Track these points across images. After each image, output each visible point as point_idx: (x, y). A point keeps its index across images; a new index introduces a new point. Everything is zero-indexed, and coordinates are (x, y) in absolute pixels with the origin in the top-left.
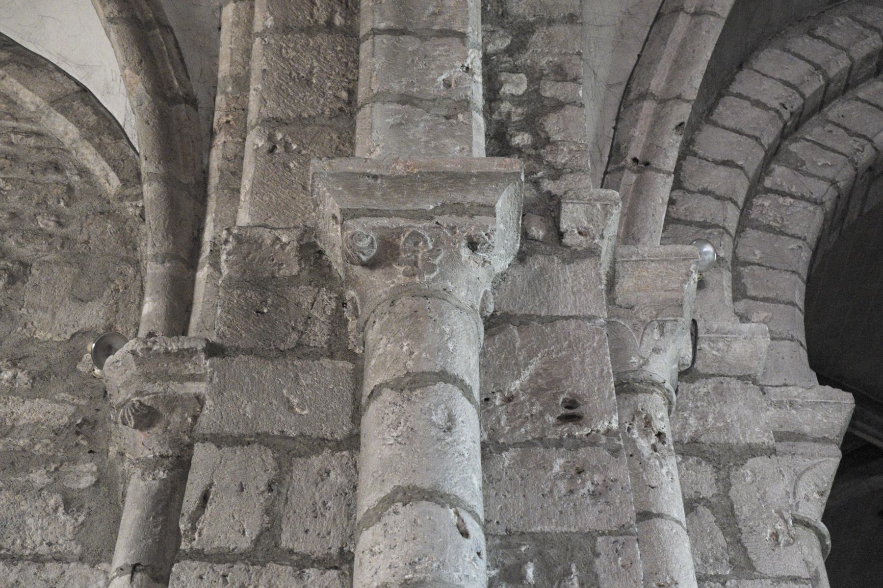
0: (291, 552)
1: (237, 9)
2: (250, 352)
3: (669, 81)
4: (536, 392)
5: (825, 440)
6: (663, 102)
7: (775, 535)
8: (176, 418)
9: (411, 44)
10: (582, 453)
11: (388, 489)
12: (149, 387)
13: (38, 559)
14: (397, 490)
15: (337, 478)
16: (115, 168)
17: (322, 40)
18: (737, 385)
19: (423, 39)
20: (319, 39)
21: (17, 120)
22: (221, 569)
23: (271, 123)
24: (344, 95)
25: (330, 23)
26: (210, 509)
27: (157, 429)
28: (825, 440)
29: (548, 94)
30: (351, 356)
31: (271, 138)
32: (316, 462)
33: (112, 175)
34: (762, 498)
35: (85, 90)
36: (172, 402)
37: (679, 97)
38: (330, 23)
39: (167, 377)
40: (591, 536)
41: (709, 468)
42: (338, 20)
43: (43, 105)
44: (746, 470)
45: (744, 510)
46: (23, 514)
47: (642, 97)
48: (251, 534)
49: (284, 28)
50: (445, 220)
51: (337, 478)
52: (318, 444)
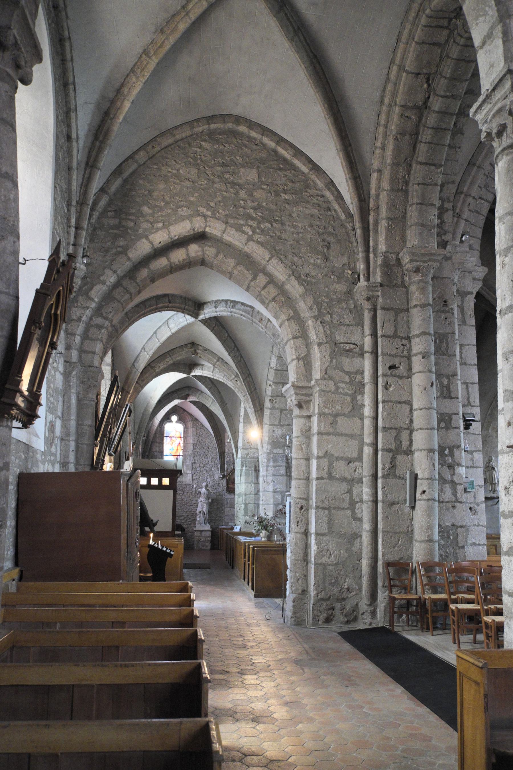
0: (400, 336)
1: (377, 175)
2: (387, 286)
3: (469, 189)
4: (439, 298)
5: (480, 280)
6: (466, 195)
7: (471, 315)
8: (373, 300)
9: (424, 207)
10: (447, 314)
11: (421, 331)
12: (369, 293)
13: (348, 325)
14: (422, 332)
15: (405, 319)
16: (343, 212)
17: (400, 194)
18: (467, 274)
19: (426, 206)
20: (399, 193)
21: (317, 190)
22: (389, 339)
23: (389, 219)
24: (404, 211)
25: (402, 188)
26: (385, 325)
27: (370, 302)
28: (480, 280)
29: (445, 206)
30: (406, 287)
31: (388, 224)
32: (401, 314)
33: (343, 214)
34: (469, 306)
35: (332, 181)
36: (373, 296)
37: (470, 195)
38: (402, 188)
39: (372, 291)
40: (447, 334)
41: (460, 298)
42: (404, 188)
43: (324, 187)
44: (467, 298)
45: (465, 309)
46: (343, 315)
47: (462, 193)
48: (393, 332)
49: (392, 190)
50: (430, 263)
51: (405, 319)
52: (402, 311)
